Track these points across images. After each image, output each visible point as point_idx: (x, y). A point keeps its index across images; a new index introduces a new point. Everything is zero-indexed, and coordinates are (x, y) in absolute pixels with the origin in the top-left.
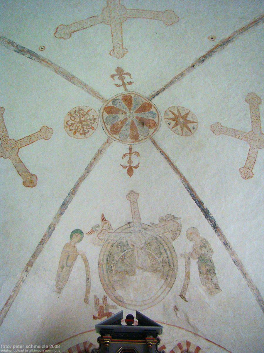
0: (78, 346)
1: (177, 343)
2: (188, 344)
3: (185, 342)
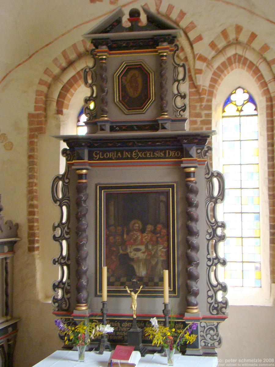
0: (74, 46)
1: (221, 29)
2: (239, 29)
3: (235, 26)
